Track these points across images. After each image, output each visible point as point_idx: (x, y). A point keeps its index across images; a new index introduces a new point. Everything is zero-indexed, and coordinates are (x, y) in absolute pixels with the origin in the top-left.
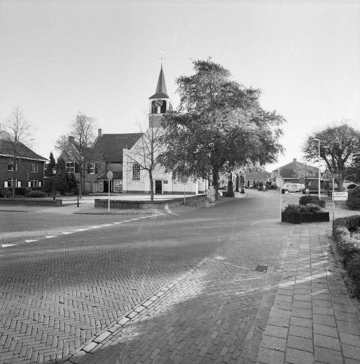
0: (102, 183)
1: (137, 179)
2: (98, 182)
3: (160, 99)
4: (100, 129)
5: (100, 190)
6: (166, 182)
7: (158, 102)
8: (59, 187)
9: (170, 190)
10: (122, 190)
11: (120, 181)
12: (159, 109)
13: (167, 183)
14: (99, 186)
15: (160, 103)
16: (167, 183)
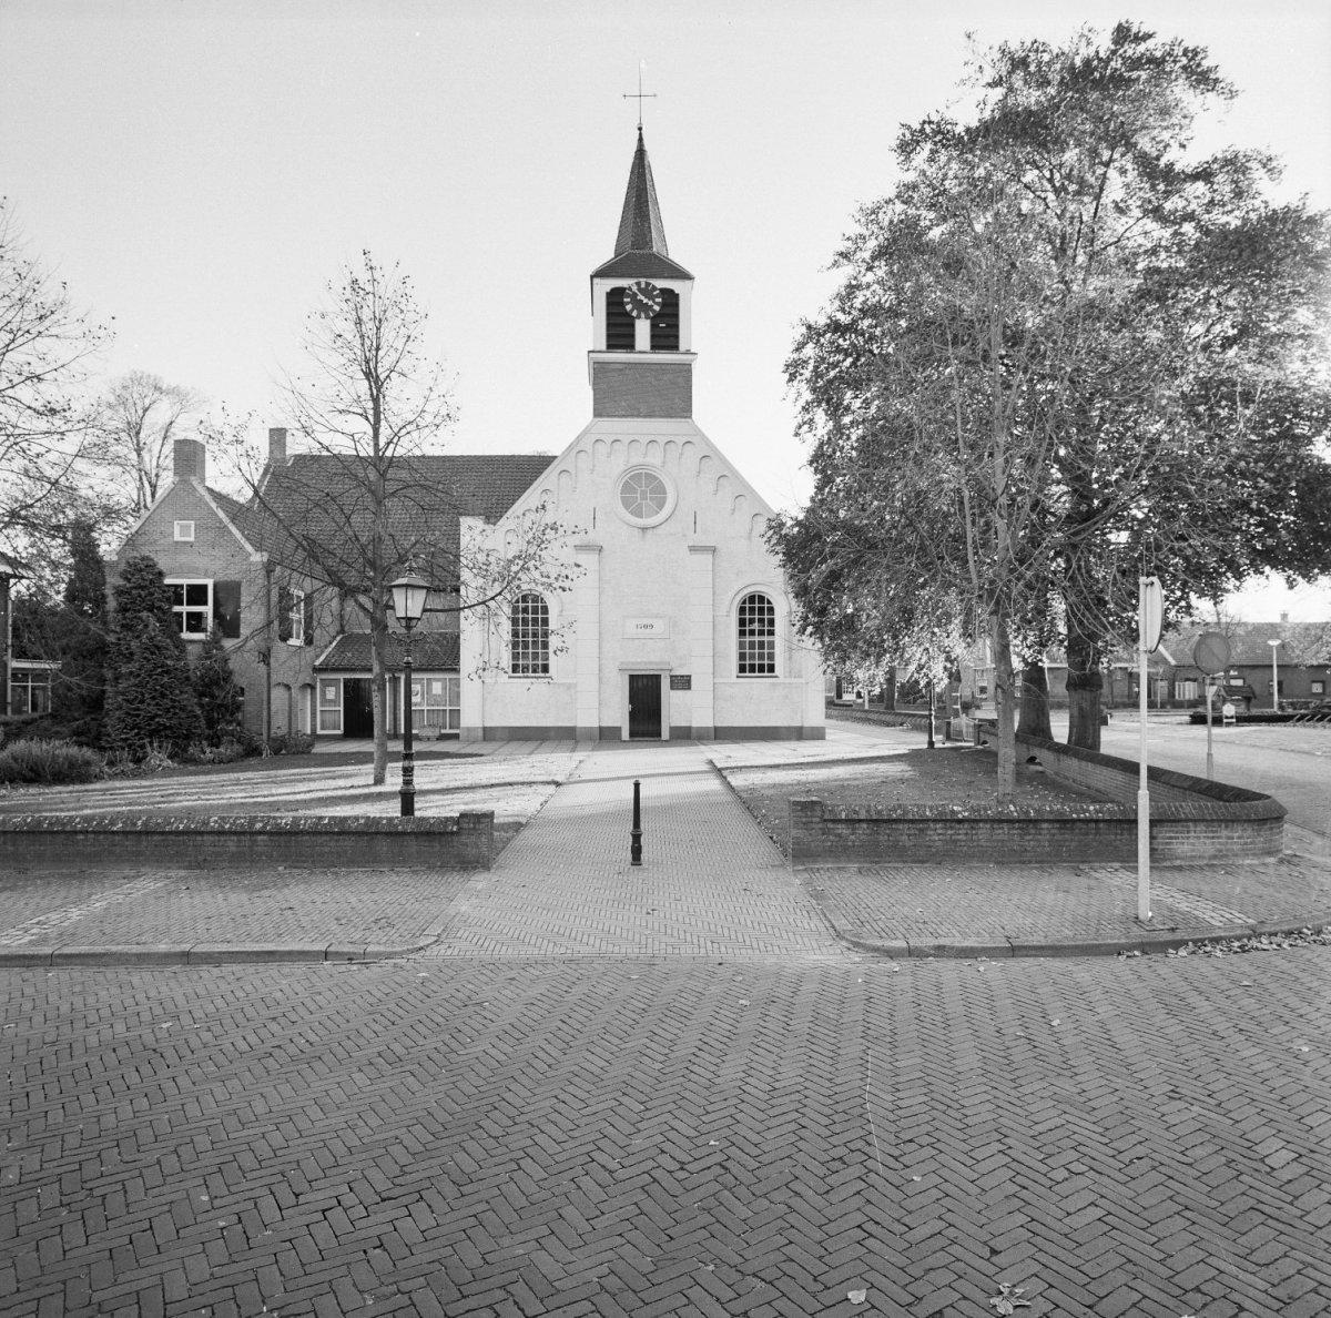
0: (337, 693)
1: (761, 669)
2: (313, 688)
3: (648, 284)
4: (277, 430)
5: (322, 729)
6: (683, 683)
7: (640, 297)
8: (152, 718)
9: (702, 719)
10: (458, 728)
11: (435, 679)
12: (643, 329)
13: (689, 688)
14: (319, 708)
15: (650, 303)
16: (689, 688)
